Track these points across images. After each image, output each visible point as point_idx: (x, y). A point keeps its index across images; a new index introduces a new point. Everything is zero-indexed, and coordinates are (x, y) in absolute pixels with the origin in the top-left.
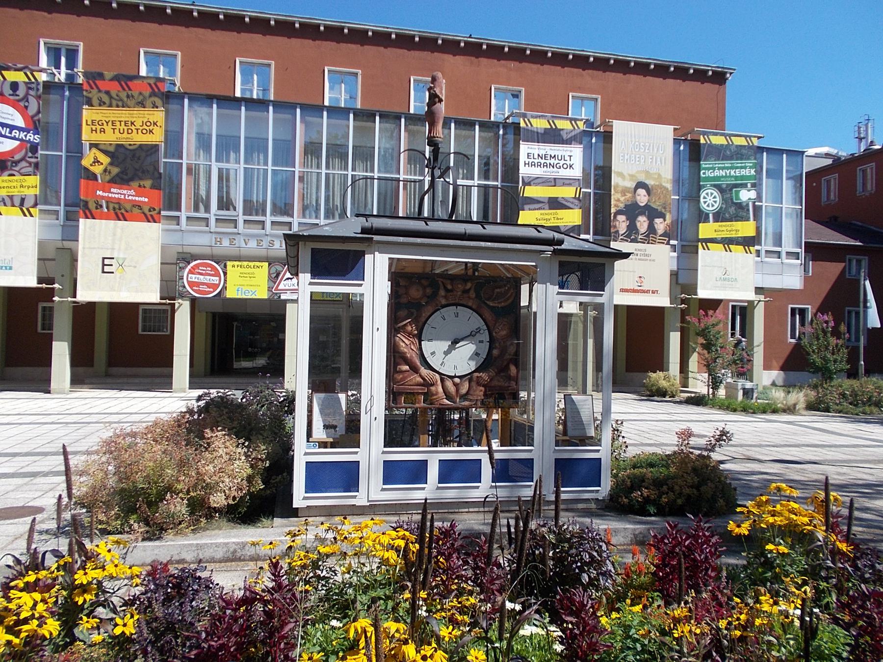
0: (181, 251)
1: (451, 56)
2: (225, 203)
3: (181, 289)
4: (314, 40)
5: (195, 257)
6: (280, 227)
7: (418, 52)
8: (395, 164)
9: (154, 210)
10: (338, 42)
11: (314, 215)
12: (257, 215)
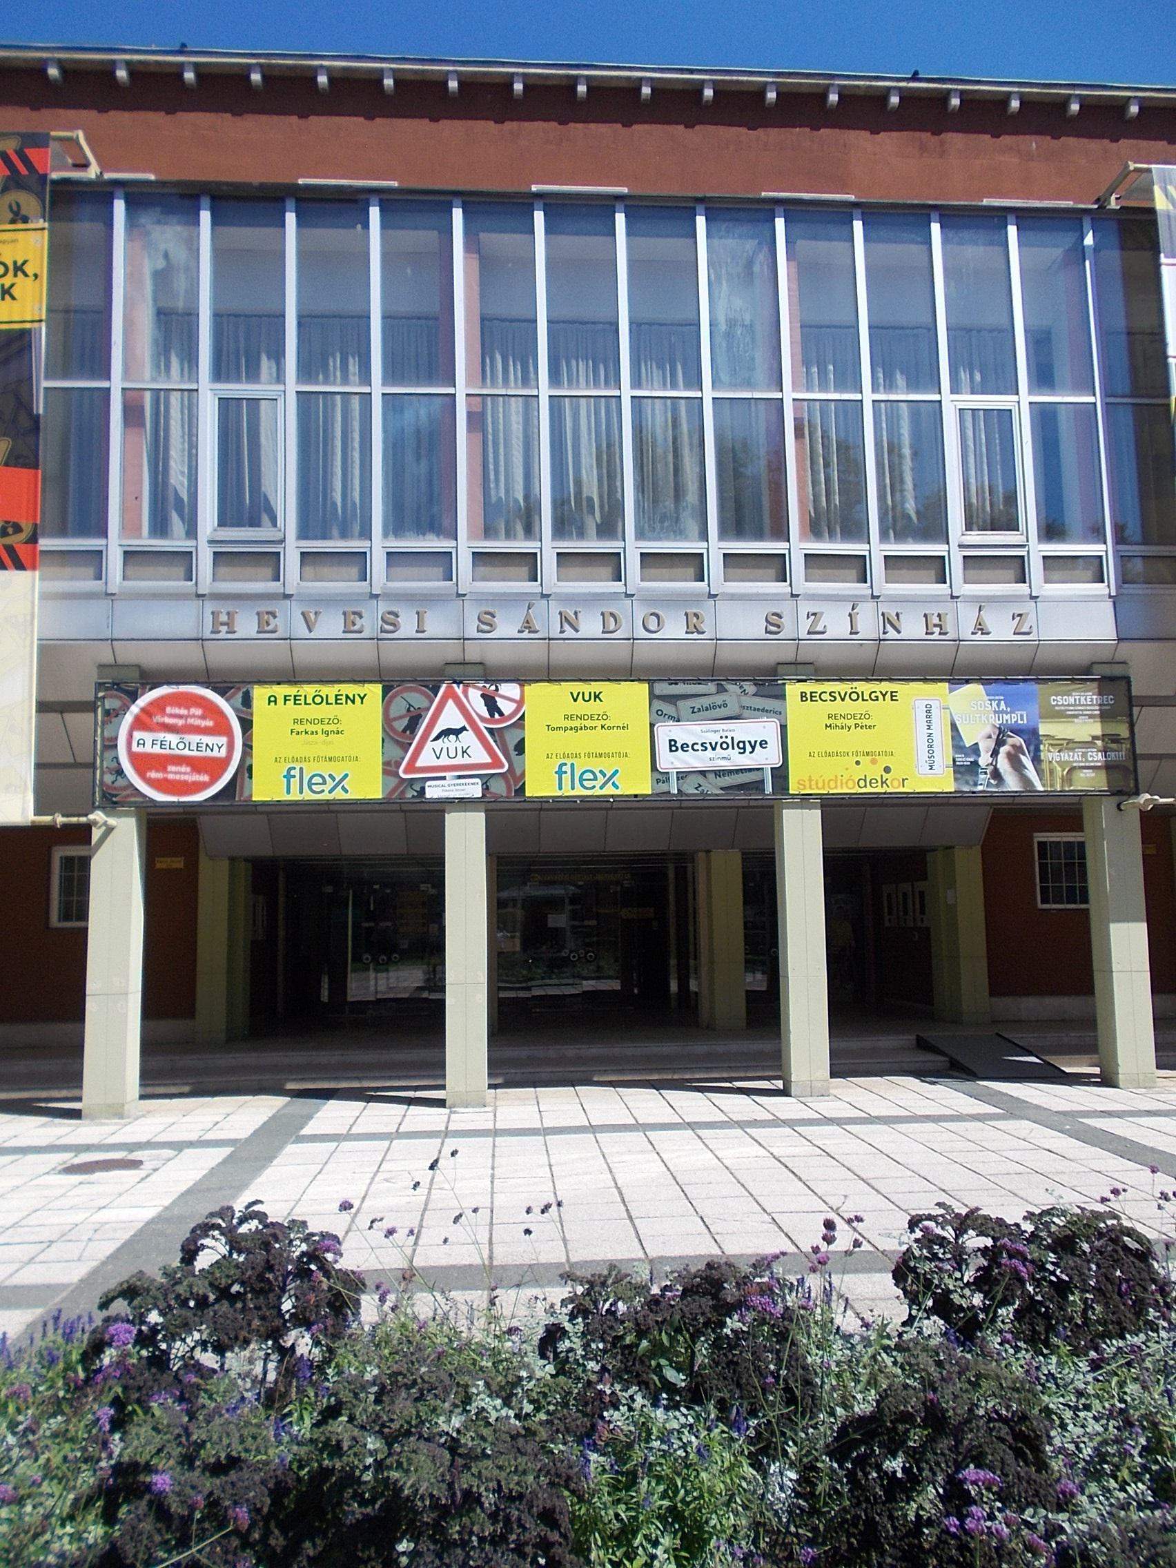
0: (107, 658)
1: (865, 134)
2: (243, 502)
3: (109, 778)
4: (500, 121)
5: (151, 679)
6: (414, 571)
7: (773, 132)
8: (761, 357)
9: (18, 529)
10: (563, 122)
11: (519, 528)
12: (344, 535)
